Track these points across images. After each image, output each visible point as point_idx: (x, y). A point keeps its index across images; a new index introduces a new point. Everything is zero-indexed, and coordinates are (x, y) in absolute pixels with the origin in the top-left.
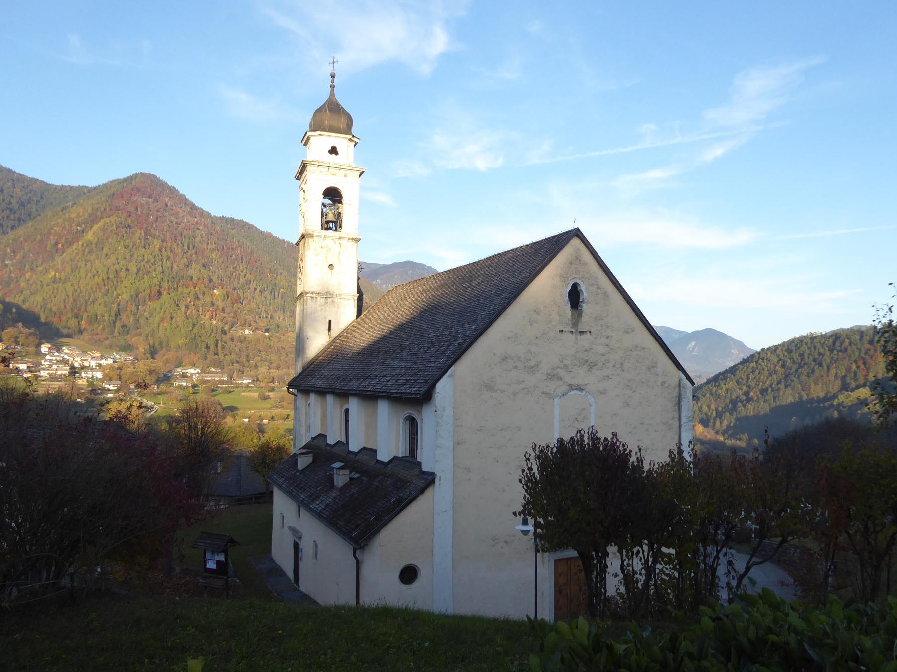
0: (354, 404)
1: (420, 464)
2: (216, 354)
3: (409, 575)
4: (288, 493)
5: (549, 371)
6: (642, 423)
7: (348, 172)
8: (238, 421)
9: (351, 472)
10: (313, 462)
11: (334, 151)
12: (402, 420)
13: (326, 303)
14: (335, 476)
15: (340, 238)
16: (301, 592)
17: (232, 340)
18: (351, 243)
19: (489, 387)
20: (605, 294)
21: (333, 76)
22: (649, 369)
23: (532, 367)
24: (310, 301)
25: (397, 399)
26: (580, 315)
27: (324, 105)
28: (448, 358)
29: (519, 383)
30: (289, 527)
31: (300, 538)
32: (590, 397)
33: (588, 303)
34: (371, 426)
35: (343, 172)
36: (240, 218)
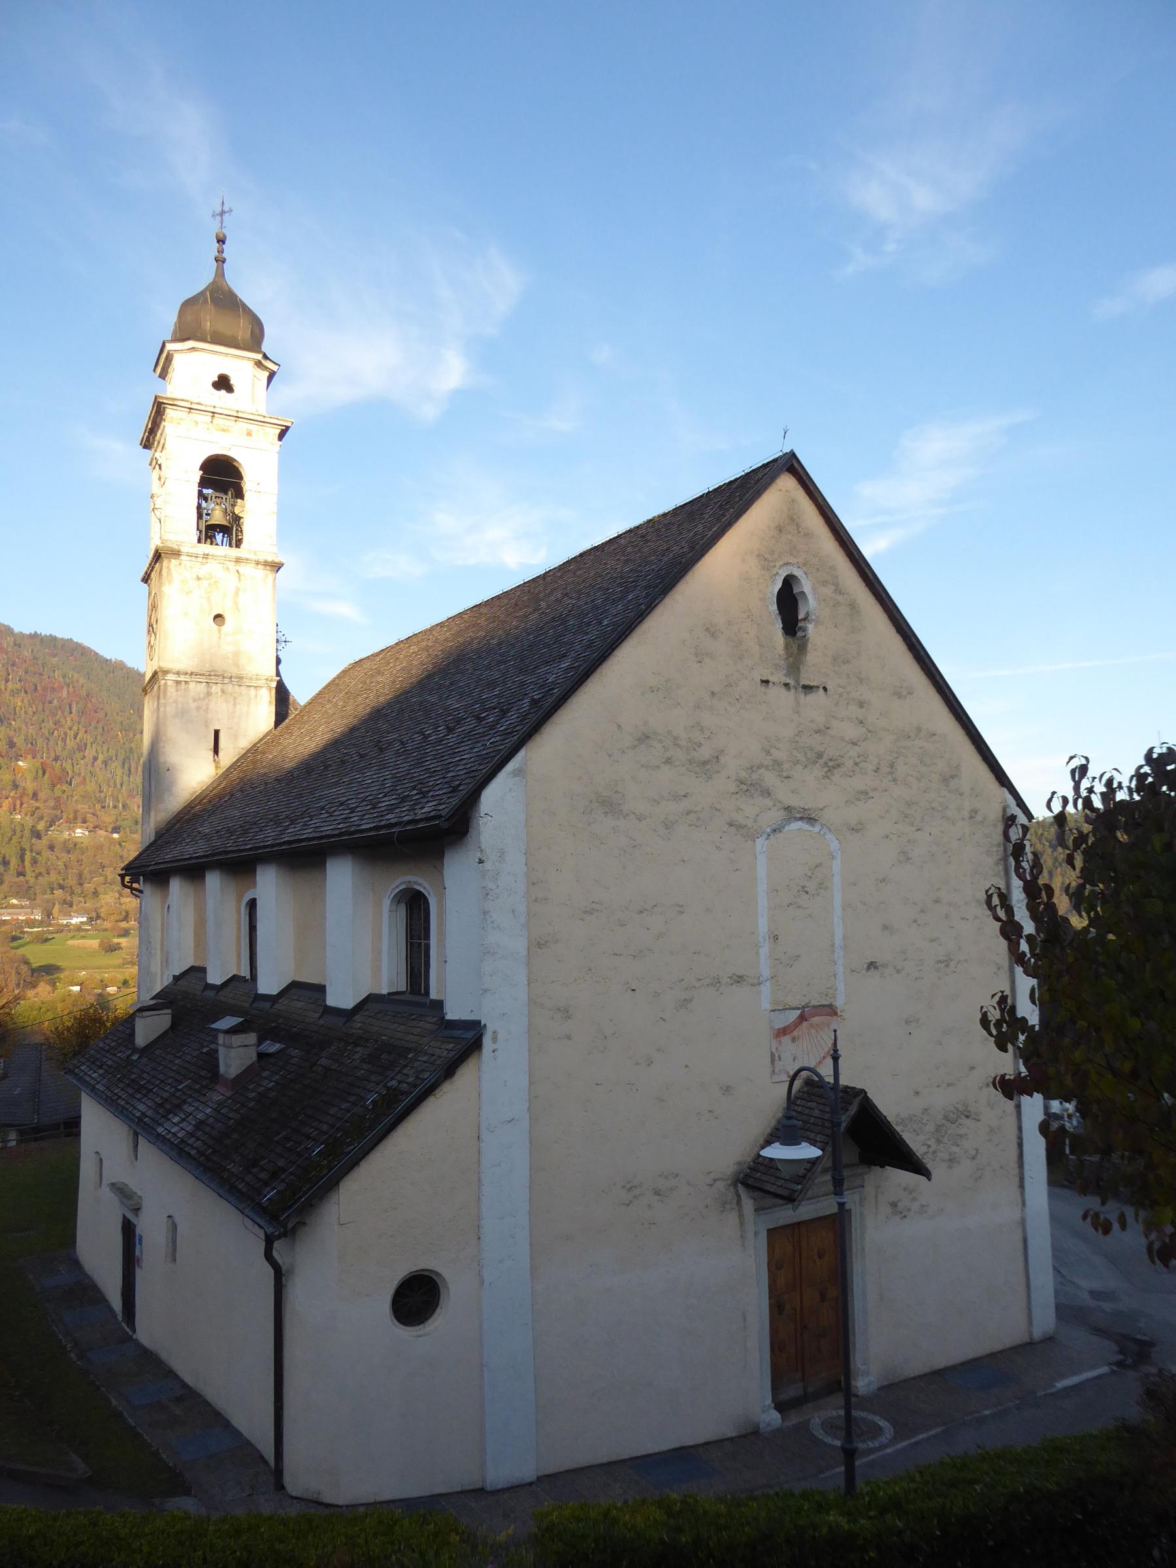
0: (268, 884)
1: (439, 1005)
2: (21, 874)
3: (417, 1298)
4: (111, 1103)
5: (743, 774)
6: (936, 901)
7: (253, 427)
8: (61, 990)
9: (260, 1042)
10: (173, 1027)
11: (223, 383)
12: (387, 903)
13: (209, 694)
14: (221, 1050)
15: (238, 560)
16: (138, 1344)
17: (51, 848)
18: (261, 572)
19: (610, 805)
20: (853, 606)
21: (221, 241)
22: (945, 780)
23: (705, 763)
24: (171, 690)
25: (378, 848)
26: (802, 648)
27: (202, 293)
28: (507, 734)
29: (676, 798)
30: (113, 1185)
31: (137, 1210)
32: (829, 836)
33: (817, 622)
34: (310, 929)
35: (243, 425)
36: (67, 637)
